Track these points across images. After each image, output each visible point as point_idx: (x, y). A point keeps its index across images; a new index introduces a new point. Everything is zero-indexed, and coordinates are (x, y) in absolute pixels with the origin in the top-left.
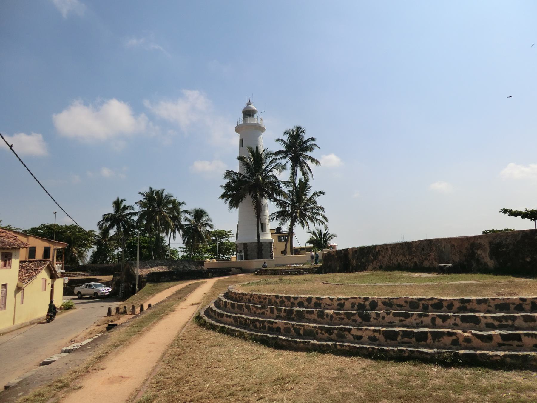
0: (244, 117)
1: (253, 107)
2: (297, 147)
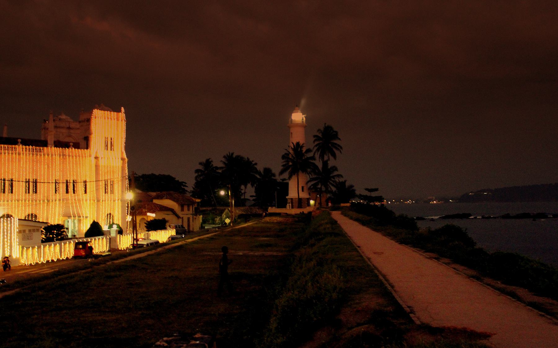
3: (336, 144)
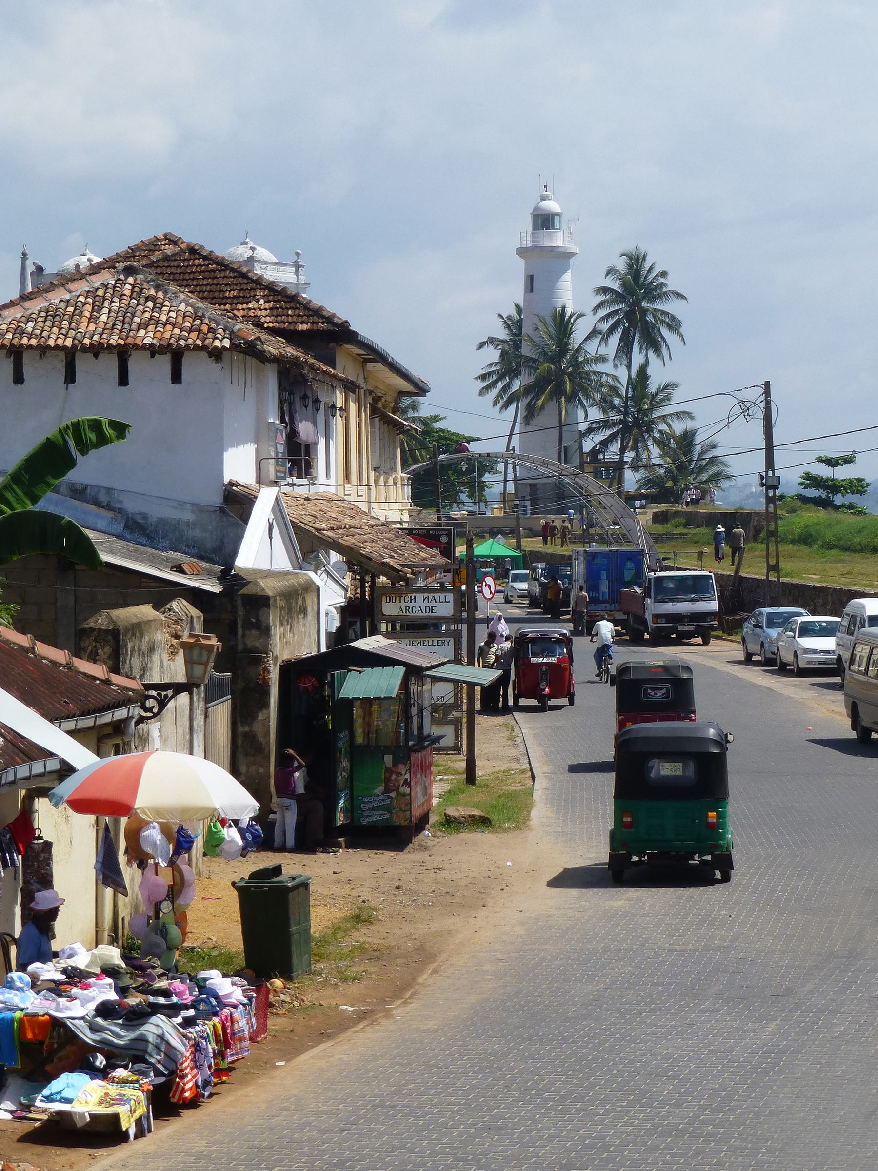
0: (535, 228)
1: (552, 206)
2: (638, 304)
3: (664, 313)
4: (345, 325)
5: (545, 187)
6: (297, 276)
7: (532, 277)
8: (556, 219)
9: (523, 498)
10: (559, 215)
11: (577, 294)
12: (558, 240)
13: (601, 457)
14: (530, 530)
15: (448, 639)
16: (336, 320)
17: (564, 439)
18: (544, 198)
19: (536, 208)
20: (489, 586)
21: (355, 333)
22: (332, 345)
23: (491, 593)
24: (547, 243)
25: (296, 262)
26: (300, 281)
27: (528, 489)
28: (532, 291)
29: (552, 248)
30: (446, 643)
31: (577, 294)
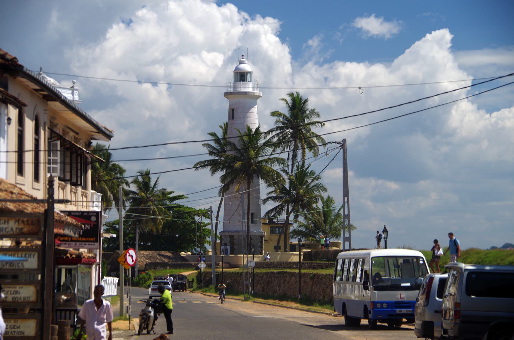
0: (236, 81)
1: (246, 67)
4: (14, 61)
5: (243, 56)
6: (73, 95)
7: (233, 110)
8: (249, 75)
9: (226, 245)
10: (250, 73)
11: (260, 119)
12: (248, 87)
13: (275, 220)
14: (229, 263)
15: (33, 253)
16: (8, 57)
17: (251, 208)
18: (241, 63)
19: (237, 68)
20: (132, 257)
21: (21, 67)
22: (5, 75)
23: (133, 261)
24: (243, 90)
25: (72, 87)
26: (75, 99)
27: (229, 239)
28: (233, 118)
29: (246, 93)
30: (32, 256)
31: (260, 119)
